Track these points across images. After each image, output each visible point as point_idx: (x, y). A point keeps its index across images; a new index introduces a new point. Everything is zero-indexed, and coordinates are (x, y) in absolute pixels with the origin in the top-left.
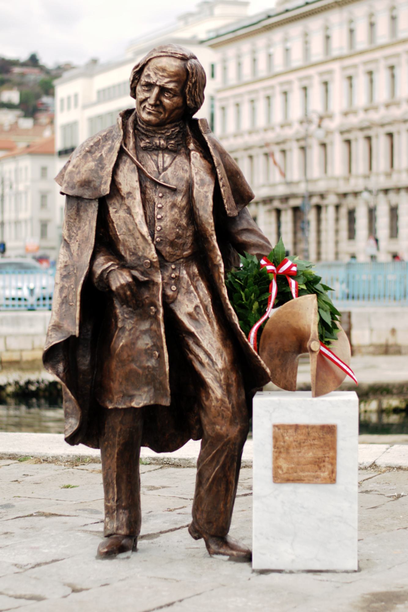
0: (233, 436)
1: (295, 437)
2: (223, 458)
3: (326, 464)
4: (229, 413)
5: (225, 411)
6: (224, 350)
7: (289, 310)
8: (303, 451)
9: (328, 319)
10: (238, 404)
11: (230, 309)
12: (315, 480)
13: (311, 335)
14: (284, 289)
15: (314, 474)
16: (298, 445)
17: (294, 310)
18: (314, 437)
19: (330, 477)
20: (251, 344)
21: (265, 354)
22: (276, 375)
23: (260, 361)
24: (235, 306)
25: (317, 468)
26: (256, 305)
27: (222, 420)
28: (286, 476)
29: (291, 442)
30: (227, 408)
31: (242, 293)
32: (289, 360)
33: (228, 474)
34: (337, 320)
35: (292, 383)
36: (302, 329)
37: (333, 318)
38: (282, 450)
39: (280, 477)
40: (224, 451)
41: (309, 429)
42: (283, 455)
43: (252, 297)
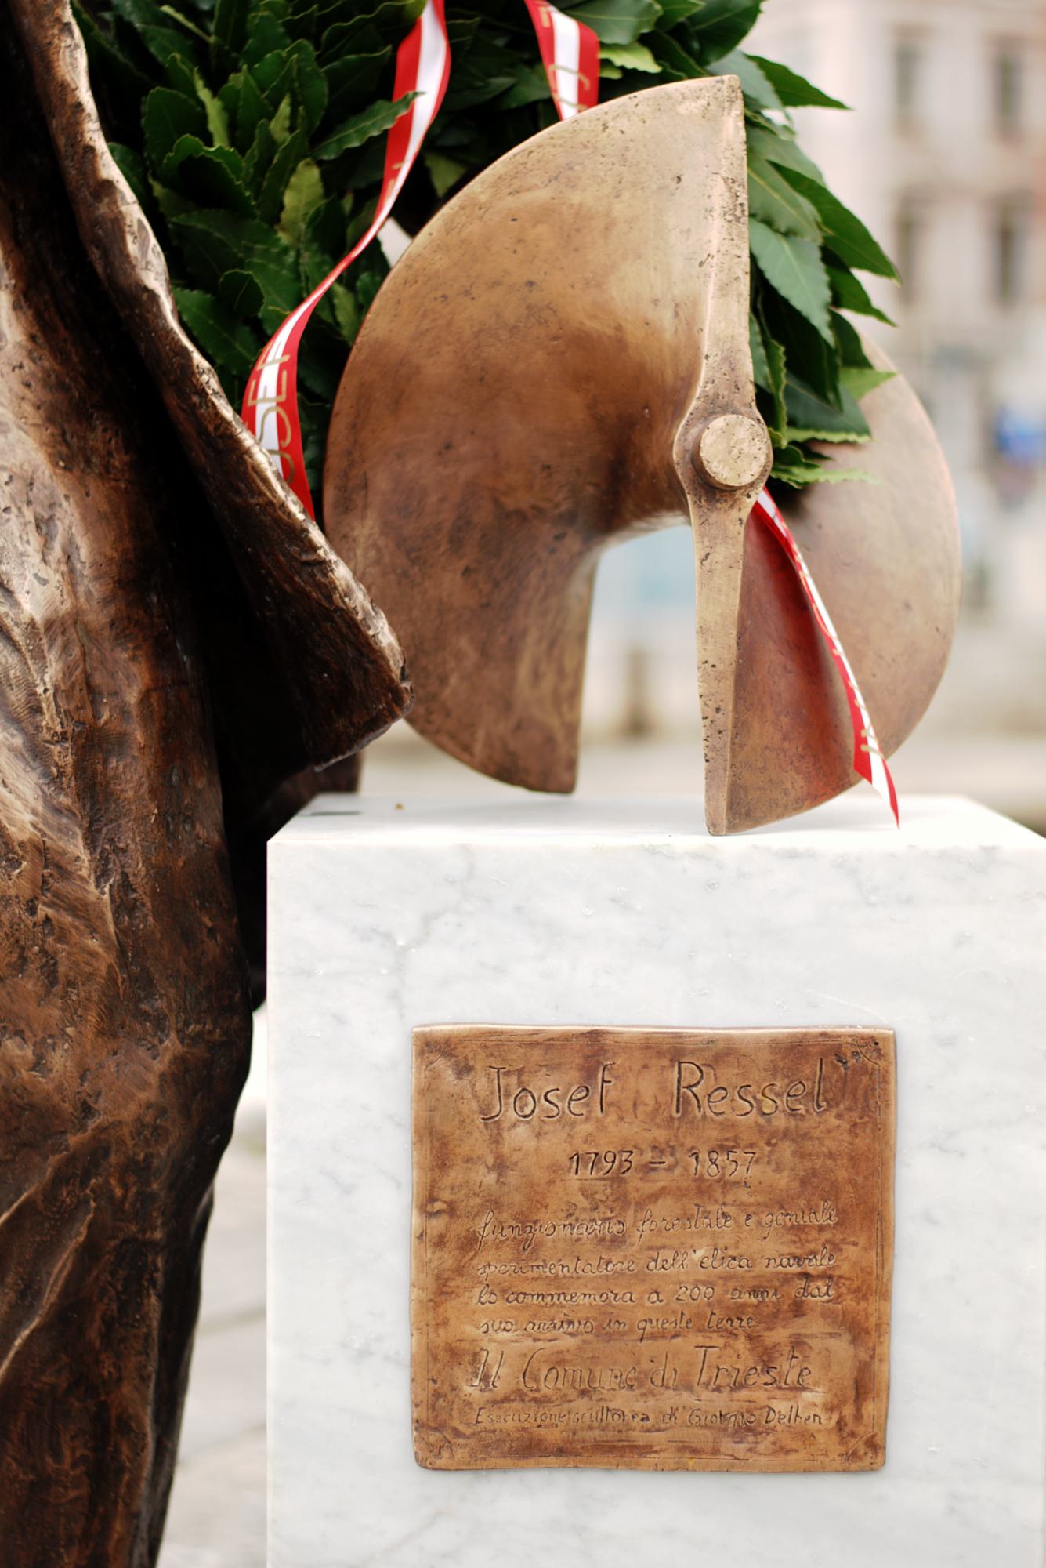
0: (128, 1113)
1: (585, 1128)
2: (61, 1265)
3: (813, 1326)
4: (94, 944)
5: (62, 937)
6: (61, 491)
7: (542, 195)
8: (641, 1233)
9: (805, 289)
10: (160, 874)
11: (108, 186)
12: (727, 1445)
13: (704, 374)
14: (502, 82)
15: (720, 1402)
16: (602, 1190)
17: (576, 198)
18: (794, 1153)
19: (840, 1424)
20: (264, 445)
21: (365, 529)
22: (443, 680)
23: (323, 565)
24: (158, 190)
25: (741, 1353)
26: (303, 190)
27: (44, 997)
28: (509, 1421)
29: (554, 1168)
30: (80, 909)
31: (204, 94)
32: (533, 578)
33: (107, 1369)
34: (864, 305)
35: (550, 740)
36: (634, 334)
37: (845, 294)
38: (484, 1225)
39: (460, 1426)
40: (66, 1217)
41: (690, 1074)
42: (493, 1265)
43: (279, 126)
